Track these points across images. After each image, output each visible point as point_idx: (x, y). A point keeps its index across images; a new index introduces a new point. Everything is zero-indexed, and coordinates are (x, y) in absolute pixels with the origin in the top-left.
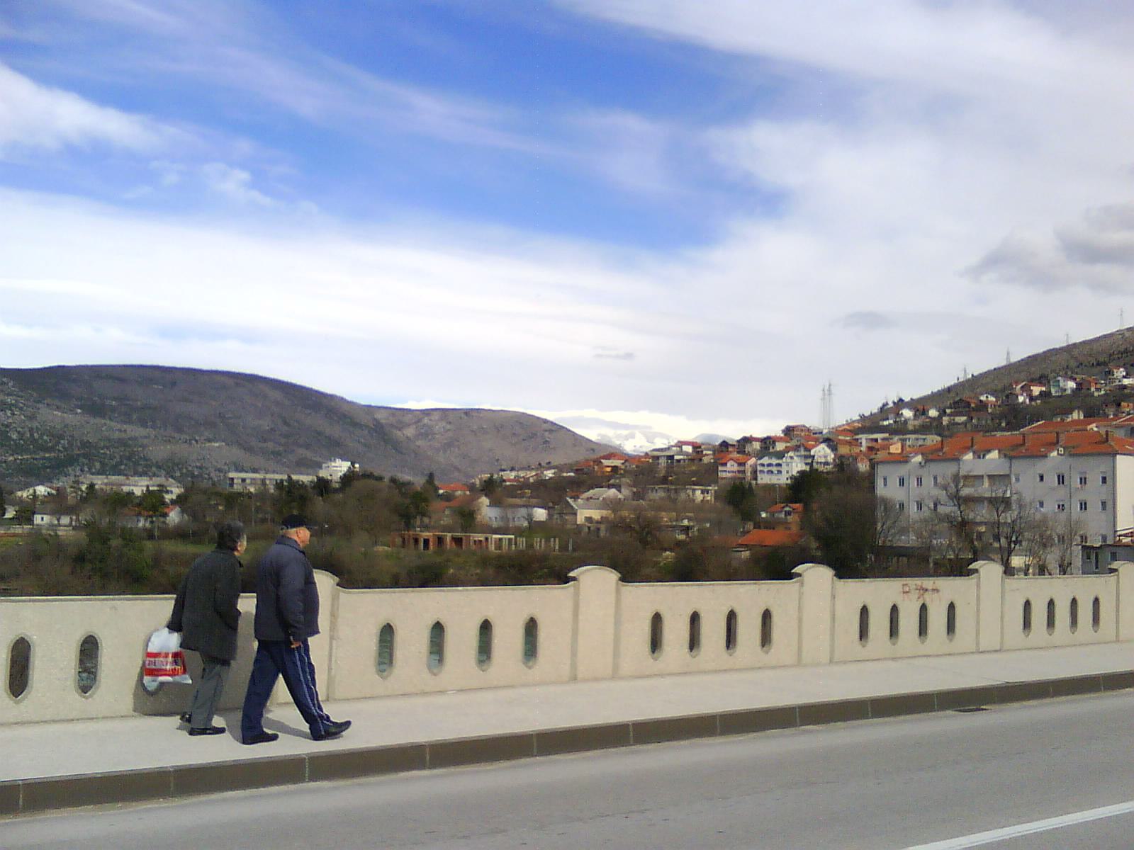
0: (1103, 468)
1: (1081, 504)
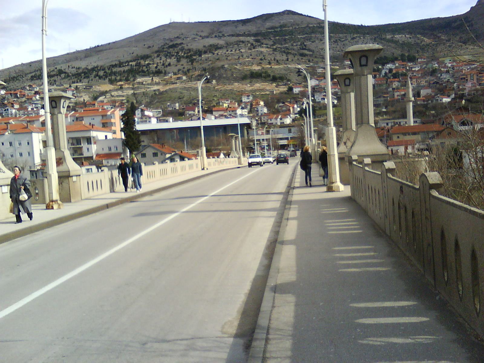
0: (27, 139)
1: (20, 154)
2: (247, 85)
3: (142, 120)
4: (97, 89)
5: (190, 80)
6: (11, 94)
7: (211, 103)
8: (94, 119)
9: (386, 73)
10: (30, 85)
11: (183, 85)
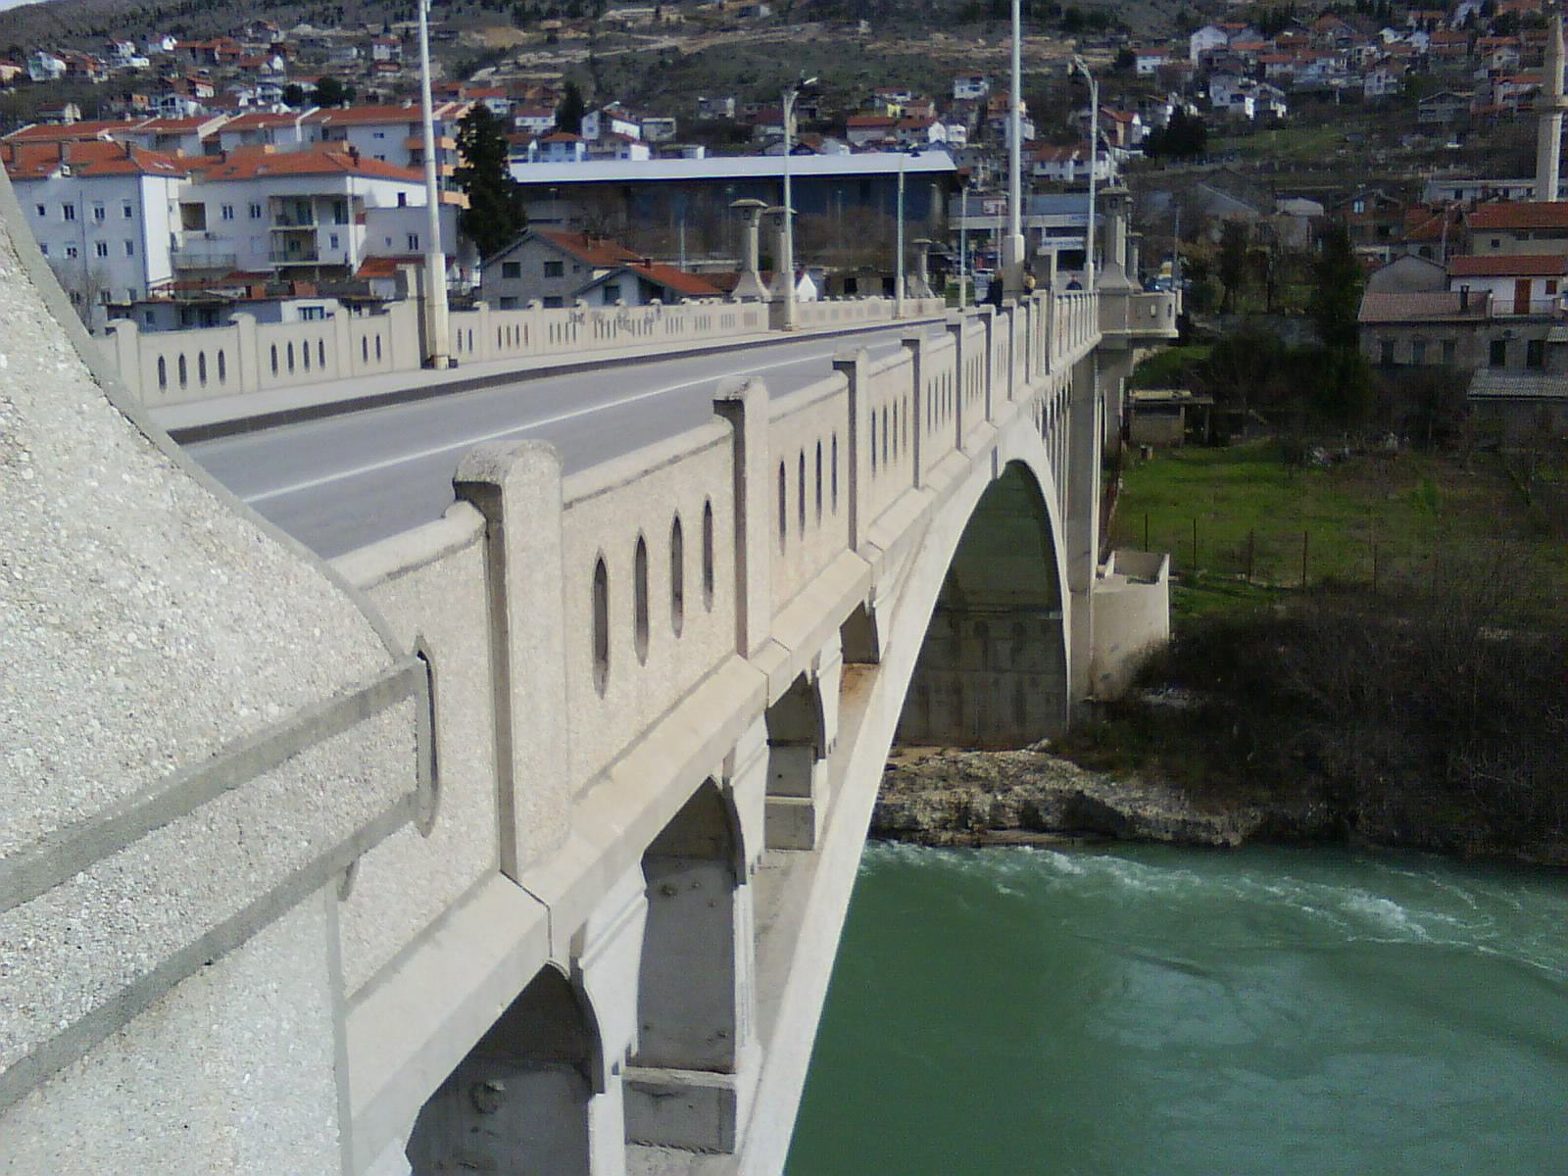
1: (99, 248)
2: (975, 41)
3: (599, 150)
4: (473, 40)
5: (781, 19)
6: (193, 50)
7: (846, 99)
8: (382, 135)
9: (1470, 15)
10: (259, 23)
11: (758, 36)
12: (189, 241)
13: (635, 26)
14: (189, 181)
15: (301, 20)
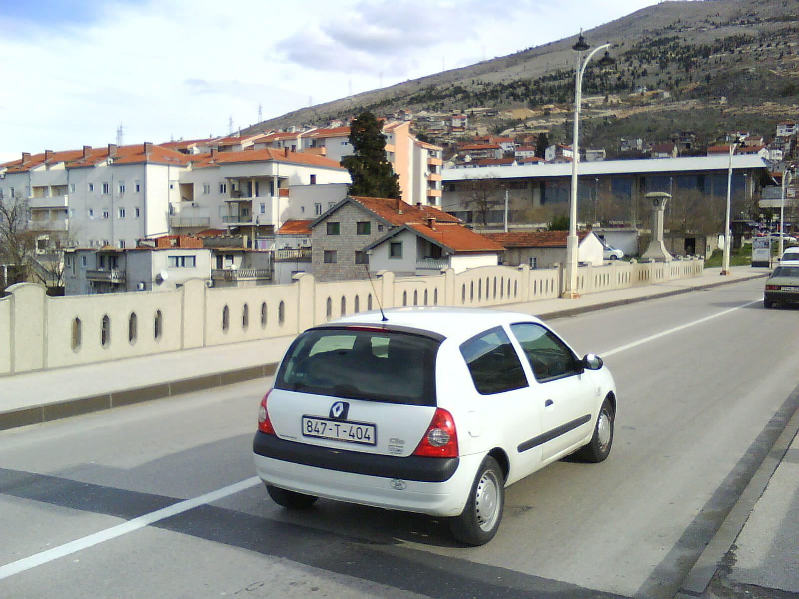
11: (662, 107)
12: (183, 208)
13: (593, 106)
14: (189, 168)
15: (424, 109)
